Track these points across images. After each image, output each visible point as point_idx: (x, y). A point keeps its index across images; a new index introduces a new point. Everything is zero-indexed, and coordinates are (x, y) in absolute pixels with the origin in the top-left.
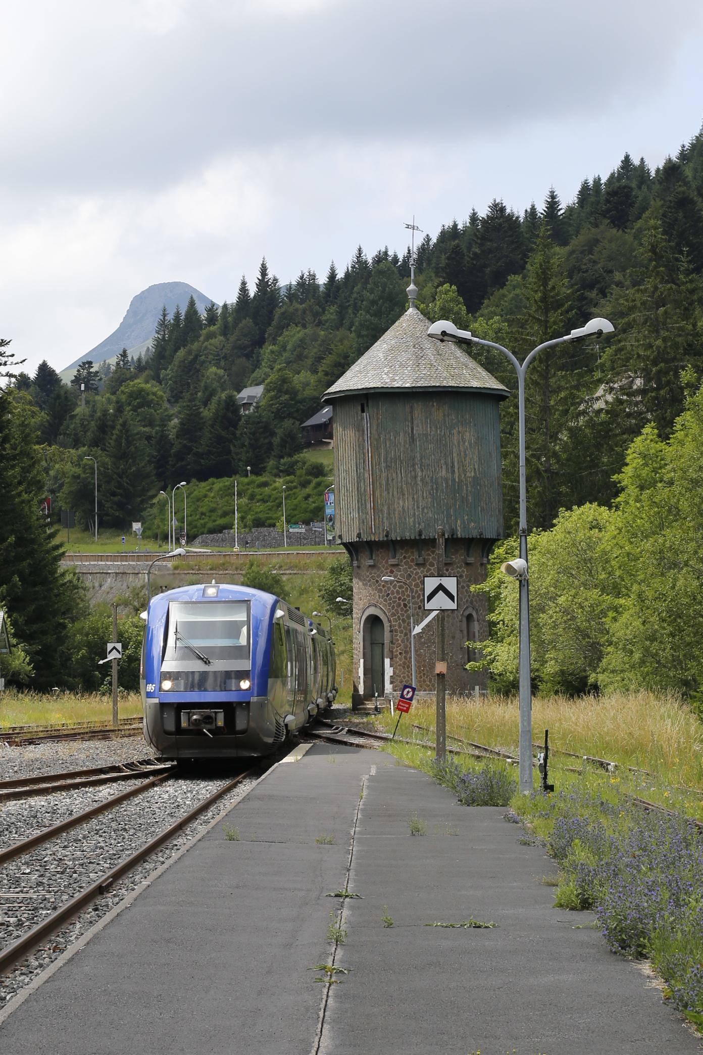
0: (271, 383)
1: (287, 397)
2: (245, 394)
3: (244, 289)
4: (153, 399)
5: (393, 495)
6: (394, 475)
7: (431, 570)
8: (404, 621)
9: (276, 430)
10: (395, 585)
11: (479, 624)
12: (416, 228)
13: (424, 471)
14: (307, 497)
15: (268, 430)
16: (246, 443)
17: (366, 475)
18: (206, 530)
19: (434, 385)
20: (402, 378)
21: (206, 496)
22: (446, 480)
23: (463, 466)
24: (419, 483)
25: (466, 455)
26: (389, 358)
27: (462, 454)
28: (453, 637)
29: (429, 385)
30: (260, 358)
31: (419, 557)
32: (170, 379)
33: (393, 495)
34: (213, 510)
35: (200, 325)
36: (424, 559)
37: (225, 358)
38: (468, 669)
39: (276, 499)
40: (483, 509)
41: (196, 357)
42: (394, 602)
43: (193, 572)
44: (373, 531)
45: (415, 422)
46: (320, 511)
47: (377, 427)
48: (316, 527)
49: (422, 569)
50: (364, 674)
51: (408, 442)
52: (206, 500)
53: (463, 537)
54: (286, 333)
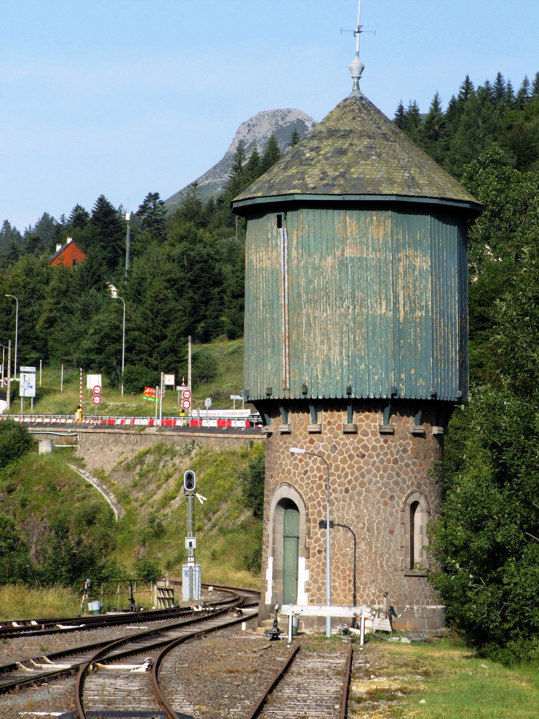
7: (363, 440)
13: (358, 307)
28: (392, 532)
44: (288, 385)
49: (351, 439)
50: (274, 578)
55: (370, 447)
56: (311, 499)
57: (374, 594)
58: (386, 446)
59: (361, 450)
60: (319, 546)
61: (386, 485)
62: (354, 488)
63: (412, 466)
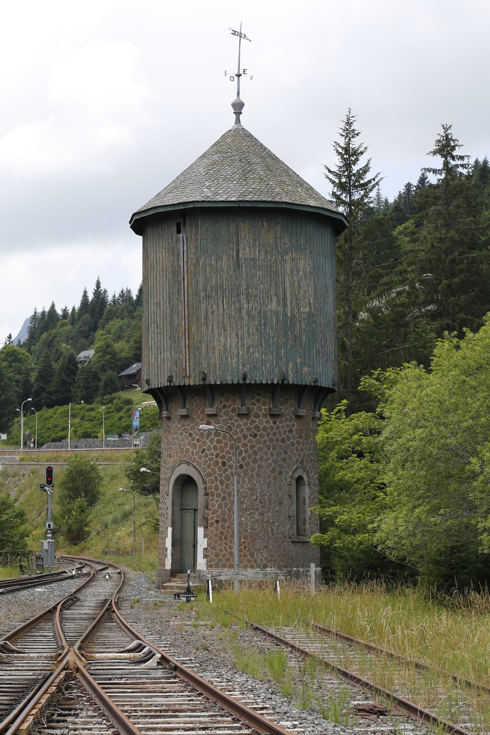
0: (99, 347)
1: (109, 356)
2: (83, 355)
3: (85, 296)
4: (21, 357)
5: (212, 331)
6: (215, 307)
7: (256, 422)
8: (222, 482)
9: (101, 377)
10: (213, 439)
11: (310, 488)
12: (243, 36)
13: (251, 302)
14: (120, 419)
15: (96, 377)
16: (81, 385)
17: (181, 307)
18: (50, 440)
19: (265, 199)
20: (226, 192)
21: (51, 417)
22: (277, 313)
23: (296, 300)
24: (245, 316)
25: (300, 286)
26: (211, 172)
27: (296, 285)
28: (281, 503)
29: (260, 199)
30: (94, 339)
31: (242, 406)
32: (37, 351)
33: (212, 331)
34: (56, 426)
35: (58, 320)
36: (248, 408)
37: (72, 338)
38: (312, 542)
39: (99, 419)
40: (318, 352)
41: (54, 338)
42: (211, 460)
43: (34, 463)
44: (188, 373)
45: (241, 245)
46: (129, 428)
47: (196, 250)
48: (127, 437)
49: (245, 421)
50: (173, 546)
51: (232, 267)
52: (52, 419)
53: (295, 383)
54: (111, 323)
55: (261, 427)
56: (209, 475)
57: (266, 559)
58: (275, 426)
59: (253, 430)
60: (216, 516)
61: (275, 462)
62: (247, 464)
63: (296, 445)
